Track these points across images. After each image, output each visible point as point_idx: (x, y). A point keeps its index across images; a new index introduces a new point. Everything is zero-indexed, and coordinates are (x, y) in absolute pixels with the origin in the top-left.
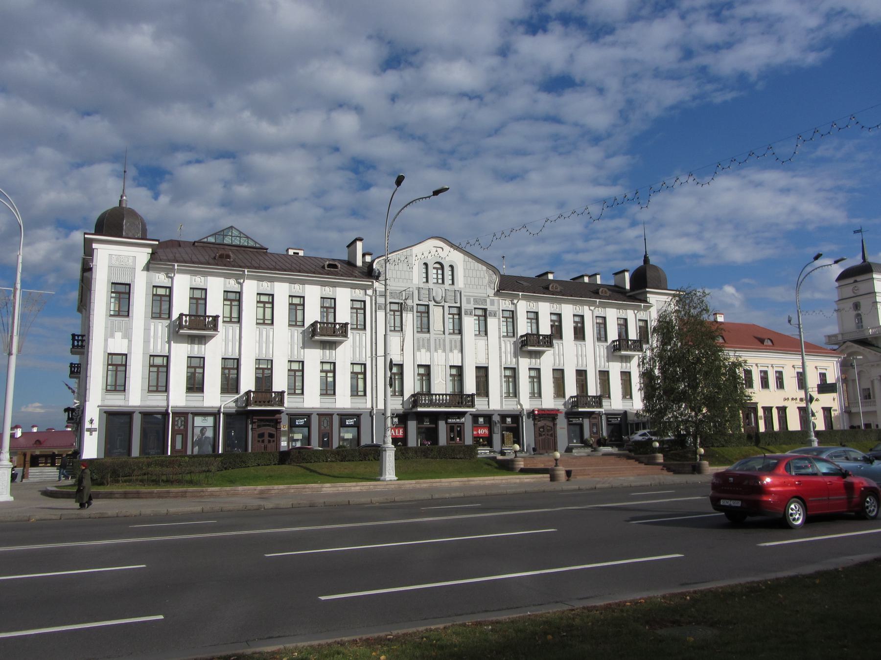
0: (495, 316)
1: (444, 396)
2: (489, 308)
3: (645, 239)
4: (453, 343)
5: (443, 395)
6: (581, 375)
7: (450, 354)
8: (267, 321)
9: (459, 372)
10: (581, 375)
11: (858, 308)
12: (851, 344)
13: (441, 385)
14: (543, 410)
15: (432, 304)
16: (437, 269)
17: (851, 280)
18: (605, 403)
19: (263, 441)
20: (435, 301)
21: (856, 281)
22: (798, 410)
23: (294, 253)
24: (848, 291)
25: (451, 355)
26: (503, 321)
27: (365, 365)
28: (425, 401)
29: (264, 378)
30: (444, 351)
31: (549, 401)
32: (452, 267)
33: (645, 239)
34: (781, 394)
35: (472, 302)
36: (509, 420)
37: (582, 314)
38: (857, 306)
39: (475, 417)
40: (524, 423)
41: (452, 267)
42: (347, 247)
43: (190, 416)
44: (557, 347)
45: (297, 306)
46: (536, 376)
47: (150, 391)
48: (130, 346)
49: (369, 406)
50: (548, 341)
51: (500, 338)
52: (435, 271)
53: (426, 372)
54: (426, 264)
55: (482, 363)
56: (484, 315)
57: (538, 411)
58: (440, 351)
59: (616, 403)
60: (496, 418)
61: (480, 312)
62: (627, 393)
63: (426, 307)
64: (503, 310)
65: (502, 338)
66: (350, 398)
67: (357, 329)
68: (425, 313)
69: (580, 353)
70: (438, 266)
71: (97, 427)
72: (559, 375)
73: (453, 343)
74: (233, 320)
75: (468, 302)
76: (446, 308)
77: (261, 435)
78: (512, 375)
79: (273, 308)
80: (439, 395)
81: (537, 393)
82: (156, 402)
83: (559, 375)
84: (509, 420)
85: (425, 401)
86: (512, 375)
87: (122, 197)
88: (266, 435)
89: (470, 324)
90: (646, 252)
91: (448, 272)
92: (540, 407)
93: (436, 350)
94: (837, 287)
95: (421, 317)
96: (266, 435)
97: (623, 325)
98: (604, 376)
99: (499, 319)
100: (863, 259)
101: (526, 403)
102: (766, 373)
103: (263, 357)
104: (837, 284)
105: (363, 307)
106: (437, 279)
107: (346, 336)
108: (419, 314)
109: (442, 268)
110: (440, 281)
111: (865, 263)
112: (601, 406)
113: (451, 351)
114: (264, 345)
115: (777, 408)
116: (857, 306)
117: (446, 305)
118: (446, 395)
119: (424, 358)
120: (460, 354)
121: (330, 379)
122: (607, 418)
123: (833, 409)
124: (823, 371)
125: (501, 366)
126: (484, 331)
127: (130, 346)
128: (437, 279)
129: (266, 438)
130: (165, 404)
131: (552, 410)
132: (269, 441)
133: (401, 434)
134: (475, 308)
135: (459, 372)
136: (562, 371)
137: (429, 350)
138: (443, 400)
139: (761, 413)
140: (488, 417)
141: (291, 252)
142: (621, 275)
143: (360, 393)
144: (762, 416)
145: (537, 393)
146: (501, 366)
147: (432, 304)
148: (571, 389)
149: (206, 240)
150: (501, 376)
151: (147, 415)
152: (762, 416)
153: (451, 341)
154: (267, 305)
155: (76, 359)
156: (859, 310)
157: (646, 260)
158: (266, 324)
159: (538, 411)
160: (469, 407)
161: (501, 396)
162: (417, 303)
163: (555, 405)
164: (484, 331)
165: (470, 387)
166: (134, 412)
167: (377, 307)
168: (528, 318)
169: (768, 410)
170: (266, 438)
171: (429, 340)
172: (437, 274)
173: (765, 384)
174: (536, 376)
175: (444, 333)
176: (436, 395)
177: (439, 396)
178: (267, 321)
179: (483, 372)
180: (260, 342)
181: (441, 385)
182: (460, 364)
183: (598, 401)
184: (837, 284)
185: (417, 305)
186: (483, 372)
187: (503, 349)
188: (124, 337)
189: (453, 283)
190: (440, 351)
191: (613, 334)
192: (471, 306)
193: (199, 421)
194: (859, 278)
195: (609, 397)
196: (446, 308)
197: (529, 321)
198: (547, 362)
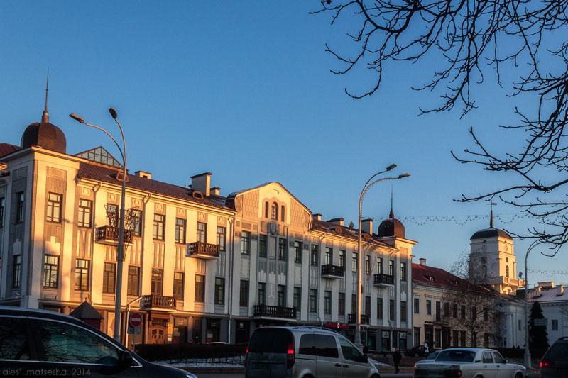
0: (307, 248)
5: (273, 307)
8: (160, 238)
9: (282, 290)
13: (272, 300)
15: (269, 234)
17: (482, 240)
19: (155, 337)
20: (272, 233)
23: (144, 176)
25: (279, 276)
27: (224, 279)
29: (157, 282)
30: (275, 273)
40: (26, 317)
42: (192, 177)
43: (105, 312)
44: (135, 243)
45: (182, 224)
47: (88, 288)
49: (226, 312)
53: (263, 288)
54: (267, 203)
55: (245, 276)
58: (262, 271)
66: (102, 294)
68: (299, 250)
74: (55, 220)
76: (278, 239)
77: (154, 332)
82: (404, 326)
83: (136, 272)
84: (241, 325)
87: (44, 112)
88: (158, 332)
90: (46, 107)
93: (279, 273)
95: (158, 225)
96: (158, 332)
102: (429, 302)
105: (59, 200)
111: (491, 229)
114: (158, 257)
118: (275, 307)
119: (262, 277)
120: (285, 277)
121: (84, 276)
124: (417, 297)
126: (299, 260)
129: (158, 334)
130: (246, 314)
132: (160, 337)
135: (282, 290)
137: (265, 271)
141: (142, 175)
142: (203, 177)
143: (220, 302)
145: (328, 311)
148: (253, 298)
149: (80, 156)
154: (56, 204)
155: (537, 322)
157: (391, 215)
160: (291, 318)
165: (168, 291)
166: (65, 307)
168: (155, 221)
169: (456, 332)
170: (158, 334)
171: (266, 263)
175: (275, 259)
176: (269, 306)
178: (160, 238)
180: (155, 254)
181: (272, 300)
182: (284, 284)
183: (170, 302)
193: (401, 334)
194: (487, 240)
195: (183, 299)
196: (278, 239)
197: (156, 223)
198: (336, 288)
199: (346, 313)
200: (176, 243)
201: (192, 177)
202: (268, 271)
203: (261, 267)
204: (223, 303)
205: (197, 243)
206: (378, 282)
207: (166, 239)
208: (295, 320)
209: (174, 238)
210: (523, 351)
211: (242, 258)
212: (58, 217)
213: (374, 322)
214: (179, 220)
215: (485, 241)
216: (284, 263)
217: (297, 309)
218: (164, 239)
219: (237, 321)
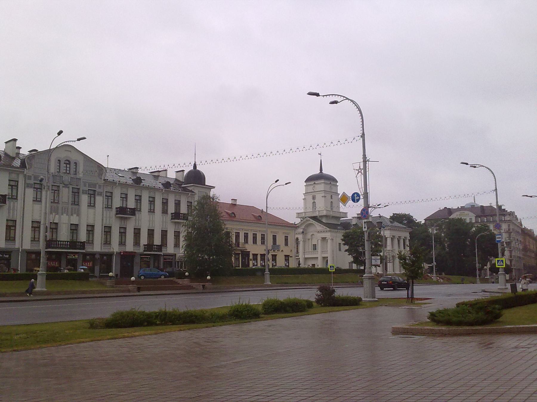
1: (66, 242)
2: (97, 189)
3: (195, 154)
4: (64, 209)
6: (151, 233)
7: (71, 216)
8: (152, 211)
9: (74, 228)
10: (151, 233)
11: (315, 199)
12: (309, 219)
13: (64, 235)
14: (127, 252)
16: (67, 164)
18: (163, 249)
21: (315, 183)
22: (271, 256)
24: (310, 189)
25: (72, 217)
26: (106, 198)
28: (54, 245)
31: (130, 247)
32: (76, 163)
33: (195, 154)
34: (264, 247)
35: (87, 185)
36: (105, 258)
37: (154, 197)
38: (314, 198)
39: (85, 255)
41: (76, 163)
46: (123, 233)
48: (79, 220)
50: (133, 212)
51: (103, 208)
52: (65, 165)
55: (91, 222)
56: (93, 194)
57: (123, 253)
58: (65, 215)
59: (170, 249)
60: (97, 256)
61: (92, 192)
62: (177, 245)
63: (16, 182)
64: (106, 192)
65: (104, 209)
67: (12, 198)
68: (56, 191)
69: (164, 220)
70: (68, 162)
71: (250, 261)
72: (137, 232)
73: (64, 209)
74: (92, 205)
75: (85, 186)
78: (107, 231)
79: (112, 199)
80: (63, 241)
81: (122, 243)
83: (137, 232)
85: (54, 245)
86: (107, 231)
89: (84, 199)
90: (195, 162)
91: (73, 166)
92: (124, 250)
93: (72, 215)
94: (305, 186)
95: (108, 199)
97: (178, 204)
98: (164, 234)
99: (103, 197)
100: (320, 171)
101: (115, 248)
103: (11, 218)
104: (305, 184)
106: (66, 170)
107: (5, 203)
108: (107, 197)
109: (69, 164)
110: (68, 172)
112: (161, 251)
113: (62, 214)
115: (261, 254)
116: (314, 198)
117: (71, 187)
118: (68, 242)
122: (165, 259)
123: (290, 256)
125: (103, 225)
126: (37, 200)
127: (79, 220)
128: (66, 170)
131: (132, 252)
133: (91, 265)
134: (34, 183)
135: (74, 228)
136: (110, 227)
138: (67, 244)
139: (251, 257)
140: (93, 255)
144: (251, 259)
145: (122, 243)
146: (102, 225)
147: (61, 186)
148: (144, 240)
150: (102, 231)
151: (102, 255)
152: (251, 259)
153: (72, 209)
156: (315, 200)
158: (13, 198)
159: (123, 253)
160: (80, 249)
161: (101, 243)
162: (52, 184)
163: (134, 250)
164: (92, 205)
165: (157, 241)
167: (27, 186)
169: (255, 256)
171: (58, 208)
172: (66, 167)
173: (255, 241)
174: (123, 233)
177: (63, 242)
178: (152, 211)
179: (91, 229)
183: (160, 248)
184: (305, 184)
185: (52, 185)
186: (91, 229)
187: (105, 215)
188: (77, 215)
189: (76, 174)
190: (65, 215)
191: (171, 209)
192: (87, 188)
197: (122, 199)
199: (142, 245)
200: (33, 201)
201: (5, 143)
202: (70, 213)
203: (54, 210)
204: (39, 241)
205: (134, 209)
206: (174, 219)
207: (96, 206)
208: (85, 251)
209: (148, 209)
210: (76, 271)
211: (88, 208)
212: (93, 203)
213: (170, 249)
214: (176, 201)
215: (315, 183)
216: (77, 207)
217: (90, 241)
218: (94, 206)
219: (29, 253)
